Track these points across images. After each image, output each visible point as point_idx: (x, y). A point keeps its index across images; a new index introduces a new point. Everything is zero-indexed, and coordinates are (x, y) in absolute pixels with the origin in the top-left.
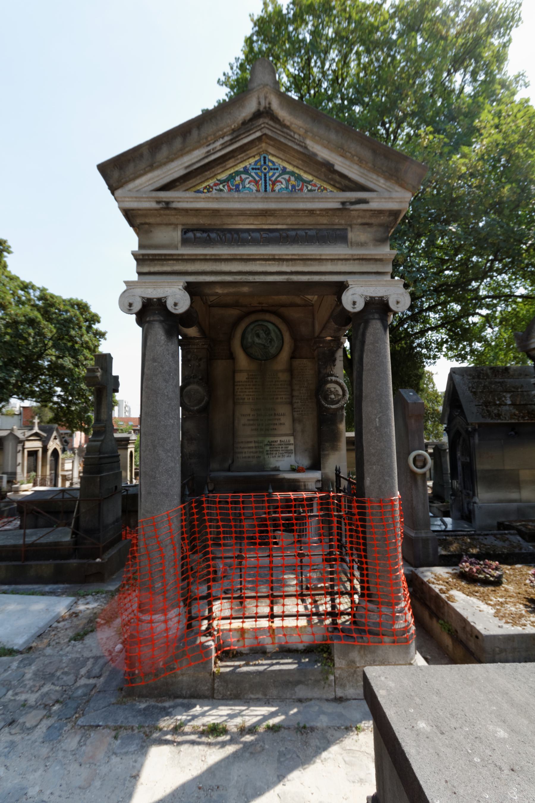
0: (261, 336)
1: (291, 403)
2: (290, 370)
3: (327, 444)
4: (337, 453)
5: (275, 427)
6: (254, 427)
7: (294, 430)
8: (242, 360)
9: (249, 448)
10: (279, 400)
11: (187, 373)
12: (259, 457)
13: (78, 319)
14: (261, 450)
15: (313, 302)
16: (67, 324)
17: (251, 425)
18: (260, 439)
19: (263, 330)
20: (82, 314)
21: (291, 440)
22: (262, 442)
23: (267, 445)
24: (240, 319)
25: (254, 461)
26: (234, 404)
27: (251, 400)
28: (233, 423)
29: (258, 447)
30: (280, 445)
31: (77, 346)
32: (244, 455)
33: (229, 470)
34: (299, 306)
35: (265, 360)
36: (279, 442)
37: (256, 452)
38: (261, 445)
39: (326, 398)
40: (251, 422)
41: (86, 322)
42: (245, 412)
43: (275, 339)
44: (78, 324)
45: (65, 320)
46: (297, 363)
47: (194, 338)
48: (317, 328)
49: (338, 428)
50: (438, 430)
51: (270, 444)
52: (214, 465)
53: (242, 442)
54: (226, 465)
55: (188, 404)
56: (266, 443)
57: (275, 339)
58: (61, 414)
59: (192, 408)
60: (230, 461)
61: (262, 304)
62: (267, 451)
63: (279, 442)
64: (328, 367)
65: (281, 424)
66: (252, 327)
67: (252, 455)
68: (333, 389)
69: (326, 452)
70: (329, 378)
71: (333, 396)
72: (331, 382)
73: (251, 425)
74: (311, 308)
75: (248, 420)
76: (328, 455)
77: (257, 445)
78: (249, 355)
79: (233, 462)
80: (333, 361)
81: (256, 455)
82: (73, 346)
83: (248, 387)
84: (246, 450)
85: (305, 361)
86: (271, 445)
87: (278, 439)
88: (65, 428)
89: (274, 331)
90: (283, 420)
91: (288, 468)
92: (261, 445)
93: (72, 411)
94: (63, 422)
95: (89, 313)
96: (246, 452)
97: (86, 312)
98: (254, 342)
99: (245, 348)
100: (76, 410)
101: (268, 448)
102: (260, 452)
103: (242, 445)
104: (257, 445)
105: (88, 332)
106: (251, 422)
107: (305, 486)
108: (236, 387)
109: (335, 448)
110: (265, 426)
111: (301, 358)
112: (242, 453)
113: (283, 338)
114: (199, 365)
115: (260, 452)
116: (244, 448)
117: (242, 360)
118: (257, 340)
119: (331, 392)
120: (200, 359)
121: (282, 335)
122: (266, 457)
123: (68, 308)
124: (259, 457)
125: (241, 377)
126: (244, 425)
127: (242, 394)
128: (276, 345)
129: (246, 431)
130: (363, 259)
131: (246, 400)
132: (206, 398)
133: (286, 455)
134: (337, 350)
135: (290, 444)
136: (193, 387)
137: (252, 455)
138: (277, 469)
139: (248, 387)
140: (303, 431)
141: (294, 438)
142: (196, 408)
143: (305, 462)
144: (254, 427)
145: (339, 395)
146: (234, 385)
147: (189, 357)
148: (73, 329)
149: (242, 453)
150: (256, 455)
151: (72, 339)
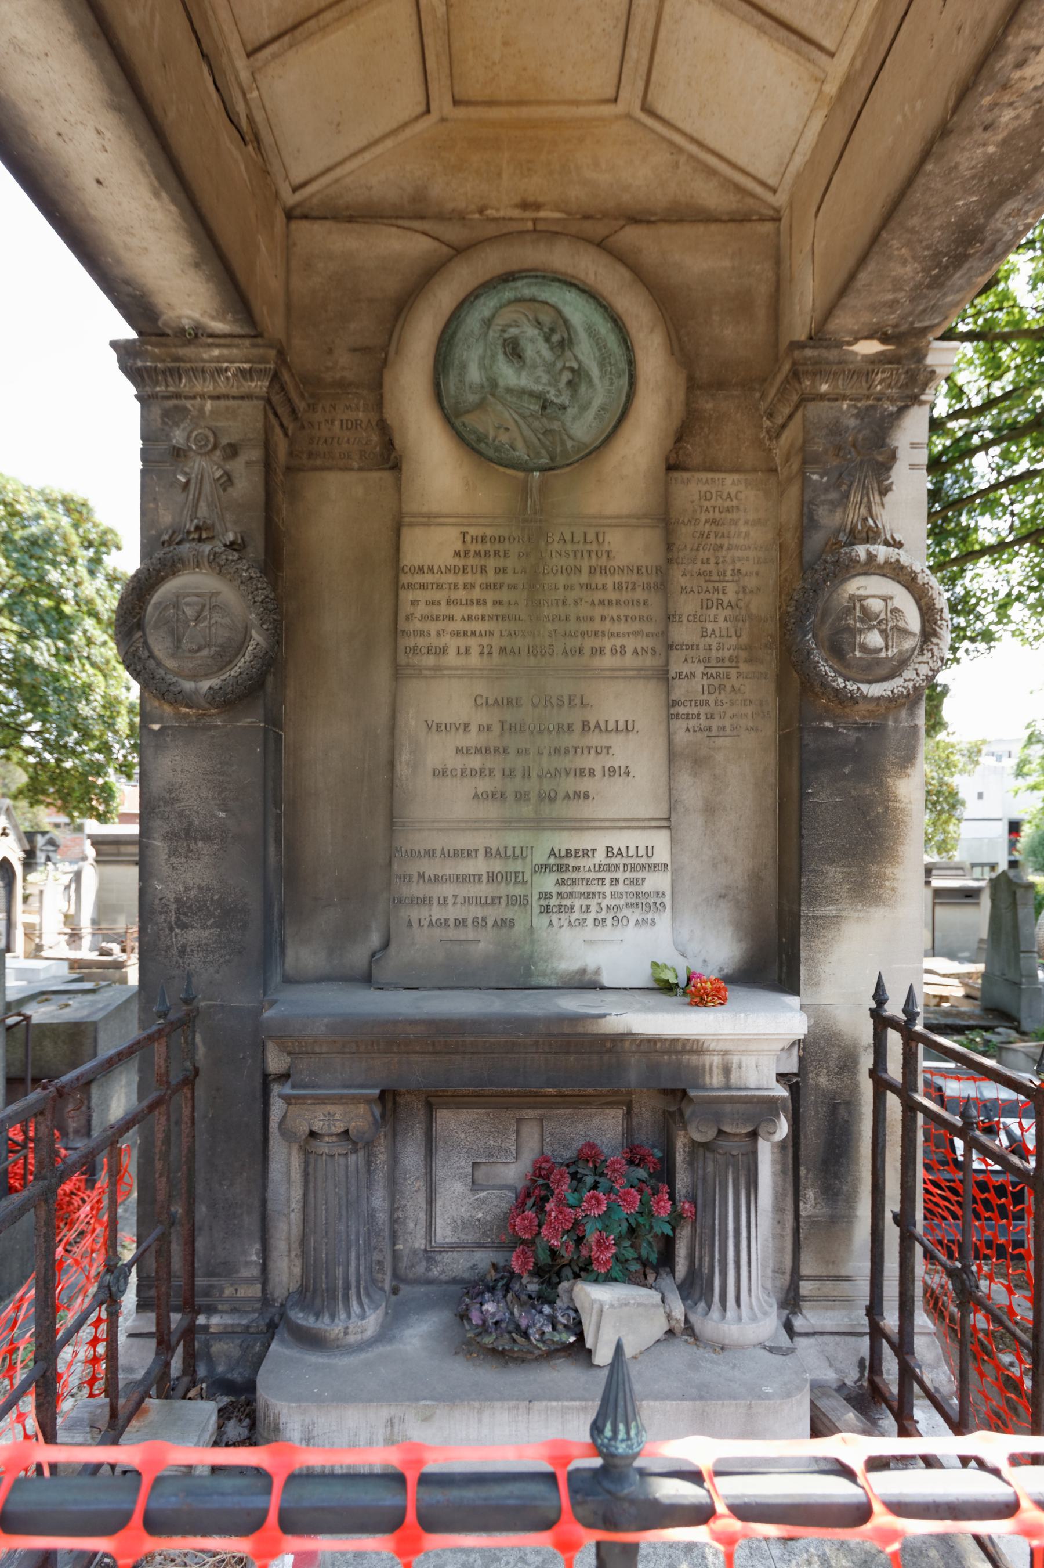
0: (529, 352)
1: (664, 676)
2: (664, 520)
3: (834, 873)
4: (878, 913)
5: (585, 784)
6: (484, 785)
7: (672, 803)
8: (438, 468)
9: (464, 879)
10: (608, 660)
11: (166, 518)
12: (507, 924)
13: (65, 538)
14: (518, 890)
15: (780, 200)
16: (37, 552)
17: (473, 773)
18: (514, 839)
19: (539, 324)
20: (76, 526)
21: (660, 844)
22: (520, 854)
23: (546, 867)
24: (428, 275)
25: (483, 944)
26: (398, 673)
27: (474, 659)
28: (392, 764)
29: (505, 877)
30: (608, 868)
31: (67, 609)
32: (437, 913)
33: (367, 979)
34: (708, 218)
35: (543, 469)
36: (600, 857)
37: (495, 901)
38: (517, 866)
39: (838, 651)
40: (475, 762)
41: (87, 548)
42: (446, 717)
43: (595, 372)
44: (65, 552)
45: (33, 542)
46: (691, 489)
47: (196, 335)
48: (807, 295)
49: (887, 798)
50: (945, 832)
51: (560, 863)
52: (304, 955)
53: (430, 854)
54: (358, 956)
55: (170, 664)
56: (540, 857)
57: (595, 372)
58: (43, 777)
59: (188, 685)
60: (375, 939)
61: (537, 206)
62: (547, 895)
63: (600, 857)
64: (855, 497)
65: (612, 771)
66: (485, 307)
67: (477, 911)
68: (876, 605)
69: (830, 910)
70: (861, 551)
71: (874, 639)
72: (871, 567)
73: (473, 773)
74: (768, 227)
75: (459, 750)
76: (837, 920)
77: (497, 866)
78: (471, 444)
79: (386, 945)
80: (876, 463)
81: (493, 913)
82: (57, 609)
83: (461, 594)
84: (447, 890)
85: (730, 482)
86: (563, 868)
87: (598, 841)
88: (53, 809)
89: (592, 332)
90: (624, 751)
91: (642, 977)
92: (517, 866)
93: (67, 771)
94: (48, 795)
95: (95, 525)
96: (447, 897)
97: (88, 520)
98: (493, 384)
99: (451, 416)
100: (75, 768)
101: (548, 882)
102: (514, 901)
103: (429, 867)
104: (497, 866)
105: (92, 573)
106: (475, 762)
107: (727, 1070)
108: (407, 596)
109: (867, 888)
110: (538, 770)
111: (712, 467)
112: (426, 901)
113: (631, 363)
114: (228, 480)
115: (514, 901)
116: (437, 879)
117: (438, 468)
118: (509, 375)
119: (867, 616)
120: (233, 451)
121: (628, 347)
122: (540, 922)
123: (43, 508)
124: (507, 924)
125: (430, 548)
126: (440, 773)
127: (433, 627)
128: (598, 401)
129: (448, 805)
130: (1011, 19)
131: (452, 659)
132: (257, 638)
133: (634, 915)
134: (902, 411)
135: (653, 867)
136: (193, 582)
137: (477, 911)
138: (587, 983)
139: (461, 594)
140: (710, 810)
141: (673, 841)
142: (205, 685)
143: (717, 949)
144: (484, 785)
145: (905, 632)
146: (397, 587)
147: (178, 437)
148: (54, 564)
149: (426, 901)
150: (493, 913)
151: (52, 592)
